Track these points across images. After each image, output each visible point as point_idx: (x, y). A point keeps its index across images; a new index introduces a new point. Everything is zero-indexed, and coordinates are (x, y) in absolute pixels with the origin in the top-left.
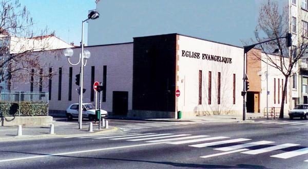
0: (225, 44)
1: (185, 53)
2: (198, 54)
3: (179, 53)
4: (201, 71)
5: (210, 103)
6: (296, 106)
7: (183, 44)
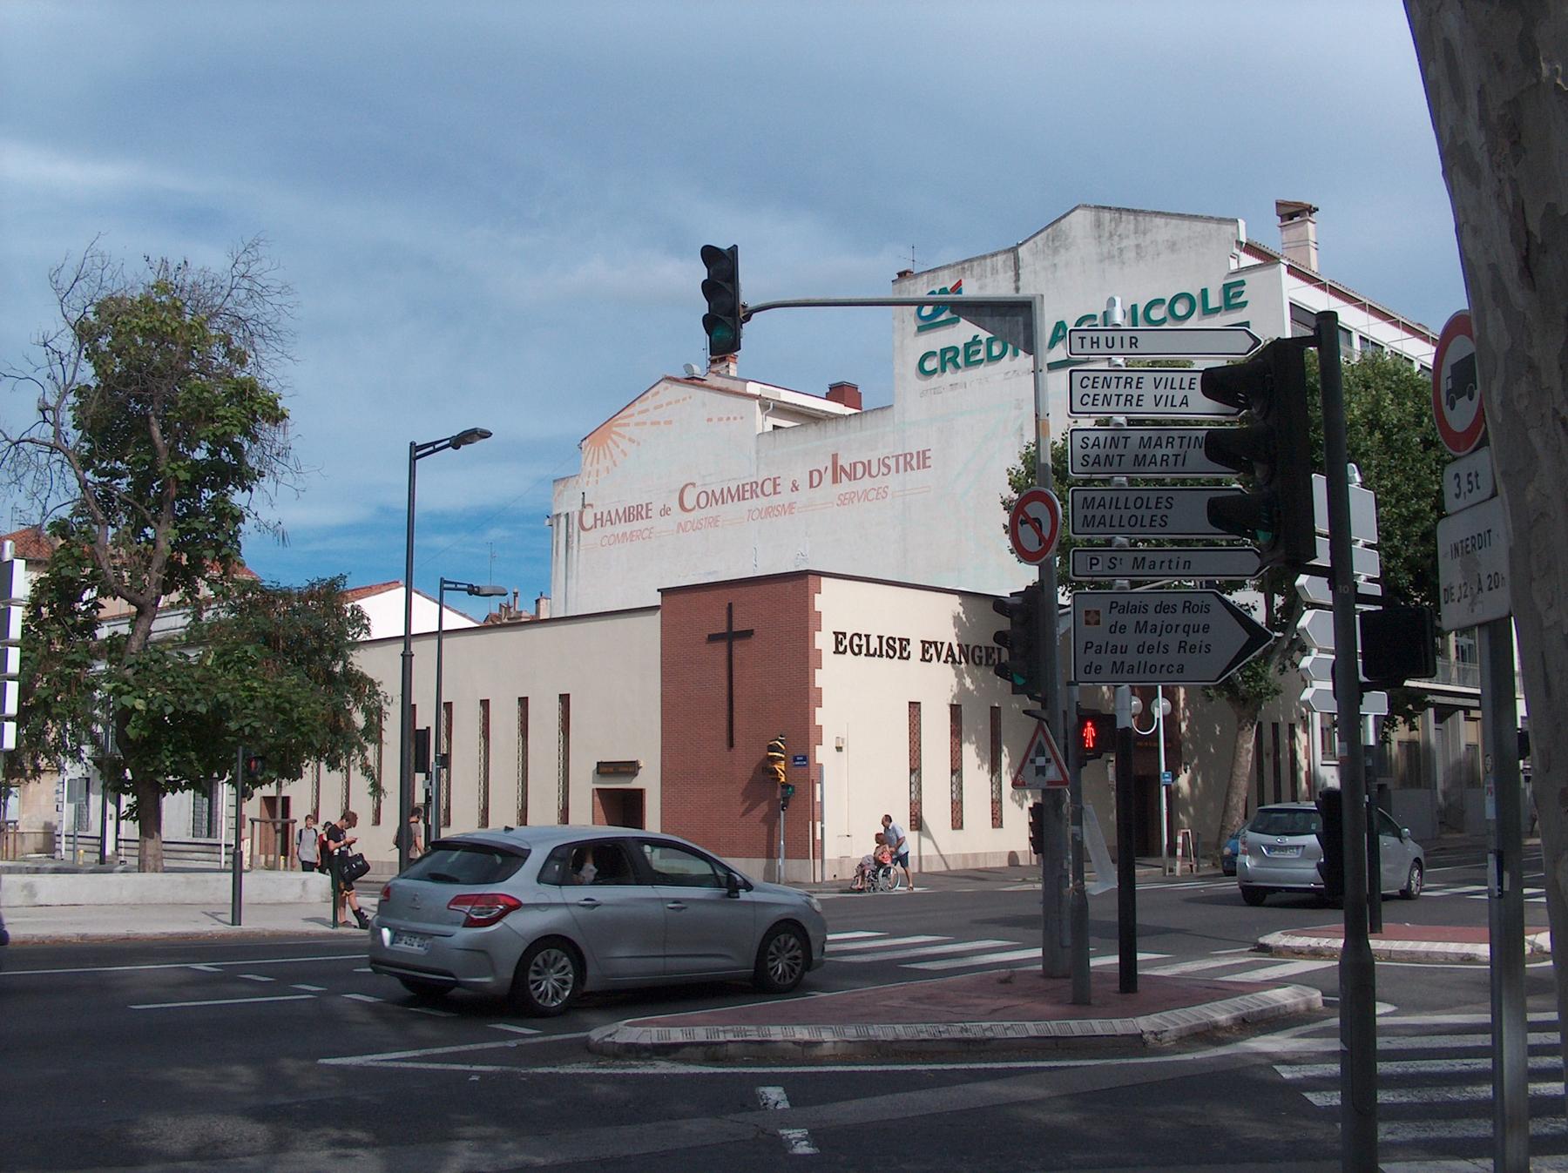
0: (1181, 216)
1: (846, 642)
2: (905, 642)
3: (823, 641)
4: (914, 706)
5: (377, 822)
6: (1254, 811)
7: (837, 607)
